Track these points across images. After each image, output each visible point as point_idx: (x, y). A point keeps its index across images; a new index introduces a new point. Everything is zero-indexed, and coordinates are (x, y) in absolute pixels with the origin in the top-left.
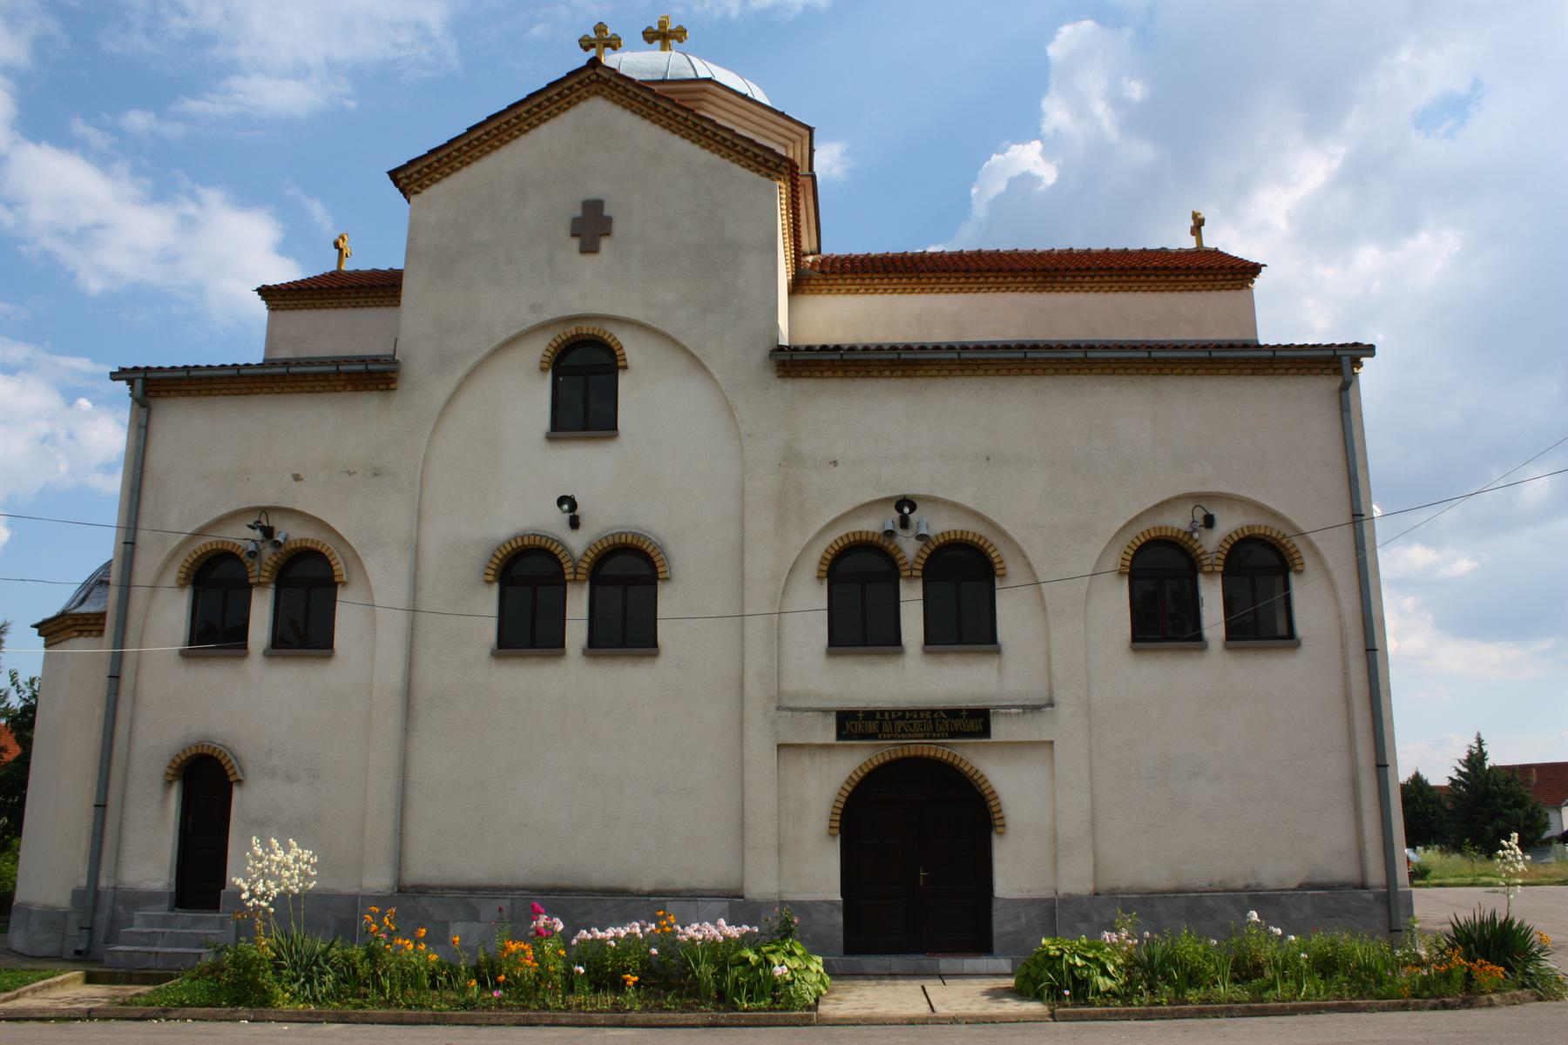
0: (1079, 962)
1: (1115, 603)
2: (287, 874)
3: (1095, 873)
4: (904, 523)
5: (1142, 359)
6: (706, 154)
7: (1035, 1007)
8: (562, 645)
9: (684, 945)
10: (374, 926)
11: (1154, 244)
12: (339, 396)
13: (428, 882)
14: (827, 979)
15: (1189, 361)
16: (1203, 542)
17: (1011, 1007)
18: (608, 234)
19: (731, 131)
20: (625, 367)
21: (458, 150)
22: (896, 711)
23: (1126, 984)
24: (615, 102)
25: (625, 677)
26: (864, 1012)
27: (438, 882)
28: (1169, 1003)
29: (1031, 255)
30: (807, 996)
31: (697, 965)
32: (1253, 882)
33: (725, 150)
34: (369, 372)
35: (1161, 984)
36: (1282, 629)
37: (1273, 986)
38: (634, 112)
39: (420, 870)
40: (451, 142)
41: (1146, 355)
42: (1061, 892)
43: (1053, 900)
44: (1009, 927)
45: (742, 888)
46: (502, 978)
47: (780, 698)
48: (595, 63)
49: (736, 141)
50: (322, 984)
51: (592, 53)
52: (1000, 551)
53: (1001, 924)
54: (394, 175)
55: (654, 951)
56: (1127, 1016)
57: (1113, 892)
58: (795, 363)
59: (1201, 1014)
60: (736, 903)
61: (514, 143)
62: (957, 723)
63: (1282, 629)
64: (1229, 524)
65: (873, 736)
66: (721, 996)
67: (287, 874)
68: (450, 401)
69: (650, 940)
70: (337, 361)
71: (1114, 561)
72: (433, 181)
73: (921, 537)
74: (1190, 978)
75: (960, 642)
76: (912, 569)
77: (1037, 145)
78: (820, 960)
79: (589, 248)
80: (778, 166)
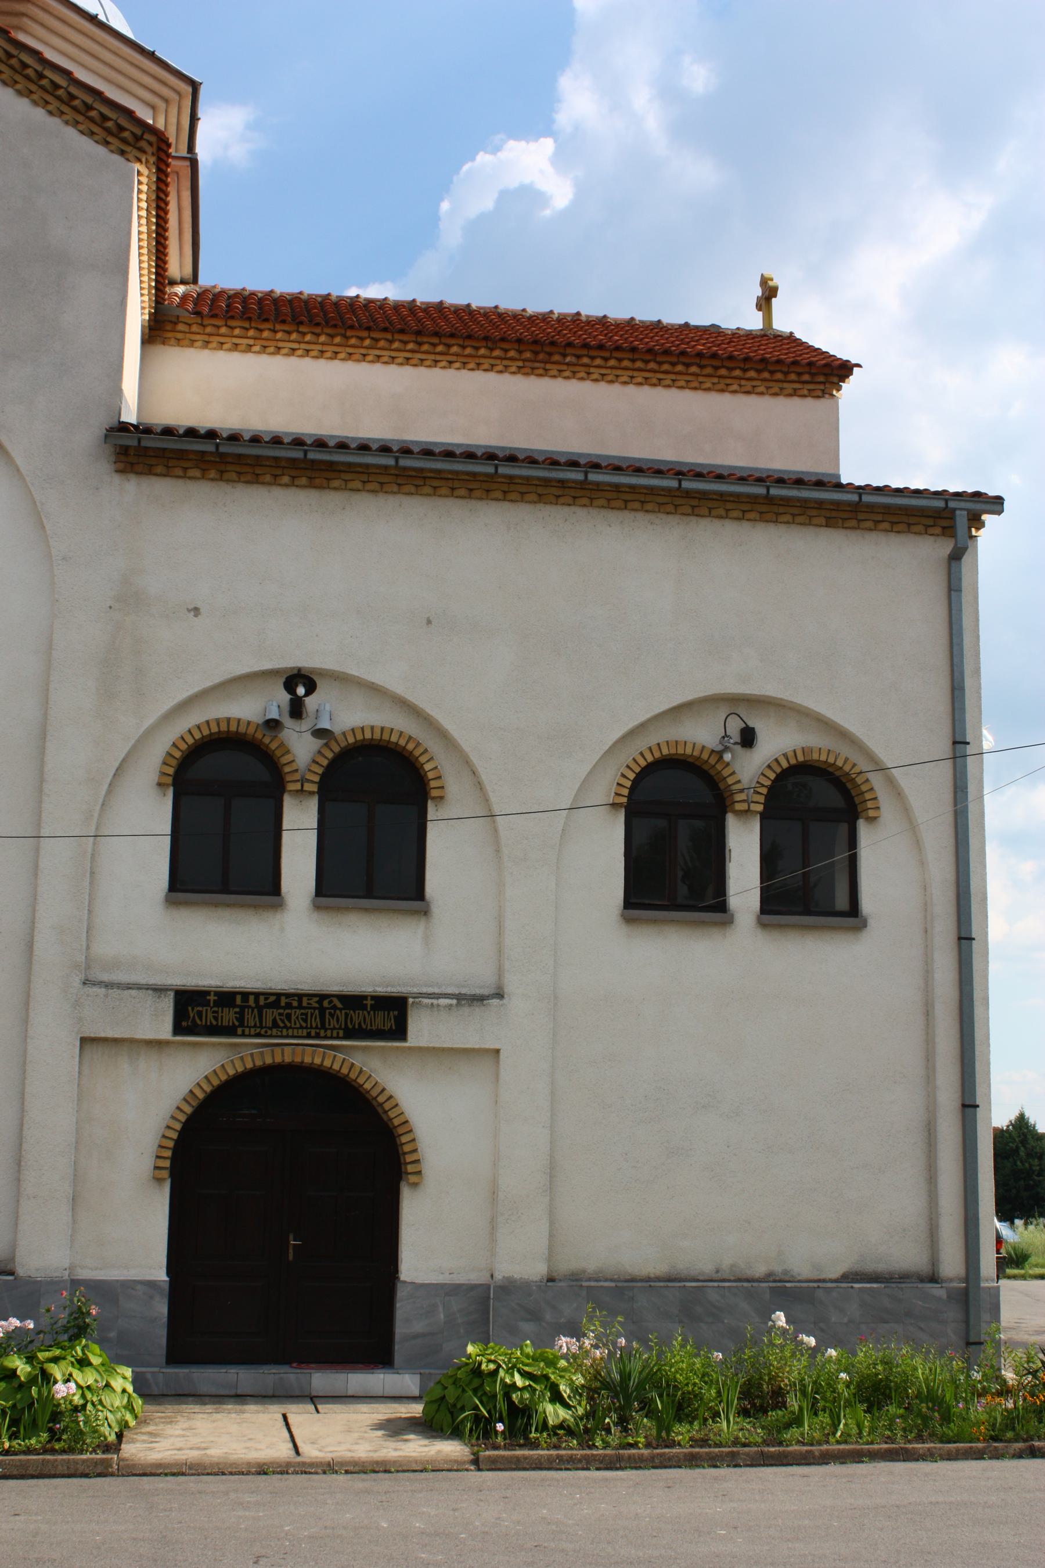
0: (519, 1381)
1: (603, 849)
3: (551, 1248)
4: (297, 710)
5: (668, 492)
6: (23, 105)
7: (451, 1449)
11: (700, 318)
14: (138, 1403)
15: (737, 498)
16: (737, 767)
17: (416, 1447)
19: (67, 74)
22: (267, 995)
23: (588, 1415)
26: (192, 1455)
28: (648, 1445)
29: (518, 318)
30: (105, 1430)
32: (778, 1269)
33: (55, 104)
35: (640, 1415)
36: (842, 902)
37: (797, 1421)
41: (674, 484)
42: (498, 1276)
43: (488, 1287)
44: (418, 1327)
47: (88, 967)
49: (73, 90)
52: (438, 762)
53: (408, 1321)
56: (586, 1464)
57: (576, 1278)
58: (143, 452)
59: (692, 1461)
62: (357, 1017)
63: (842, 902)
64: (777, 743)
65: (229, 1031)
71: (608, 785)
73: (319, 733)
74: (680, 1407)
75: (369, 894)
76: (303, 781)
77: (548, 145)
78: (128, 1372)
80: (138, 138)
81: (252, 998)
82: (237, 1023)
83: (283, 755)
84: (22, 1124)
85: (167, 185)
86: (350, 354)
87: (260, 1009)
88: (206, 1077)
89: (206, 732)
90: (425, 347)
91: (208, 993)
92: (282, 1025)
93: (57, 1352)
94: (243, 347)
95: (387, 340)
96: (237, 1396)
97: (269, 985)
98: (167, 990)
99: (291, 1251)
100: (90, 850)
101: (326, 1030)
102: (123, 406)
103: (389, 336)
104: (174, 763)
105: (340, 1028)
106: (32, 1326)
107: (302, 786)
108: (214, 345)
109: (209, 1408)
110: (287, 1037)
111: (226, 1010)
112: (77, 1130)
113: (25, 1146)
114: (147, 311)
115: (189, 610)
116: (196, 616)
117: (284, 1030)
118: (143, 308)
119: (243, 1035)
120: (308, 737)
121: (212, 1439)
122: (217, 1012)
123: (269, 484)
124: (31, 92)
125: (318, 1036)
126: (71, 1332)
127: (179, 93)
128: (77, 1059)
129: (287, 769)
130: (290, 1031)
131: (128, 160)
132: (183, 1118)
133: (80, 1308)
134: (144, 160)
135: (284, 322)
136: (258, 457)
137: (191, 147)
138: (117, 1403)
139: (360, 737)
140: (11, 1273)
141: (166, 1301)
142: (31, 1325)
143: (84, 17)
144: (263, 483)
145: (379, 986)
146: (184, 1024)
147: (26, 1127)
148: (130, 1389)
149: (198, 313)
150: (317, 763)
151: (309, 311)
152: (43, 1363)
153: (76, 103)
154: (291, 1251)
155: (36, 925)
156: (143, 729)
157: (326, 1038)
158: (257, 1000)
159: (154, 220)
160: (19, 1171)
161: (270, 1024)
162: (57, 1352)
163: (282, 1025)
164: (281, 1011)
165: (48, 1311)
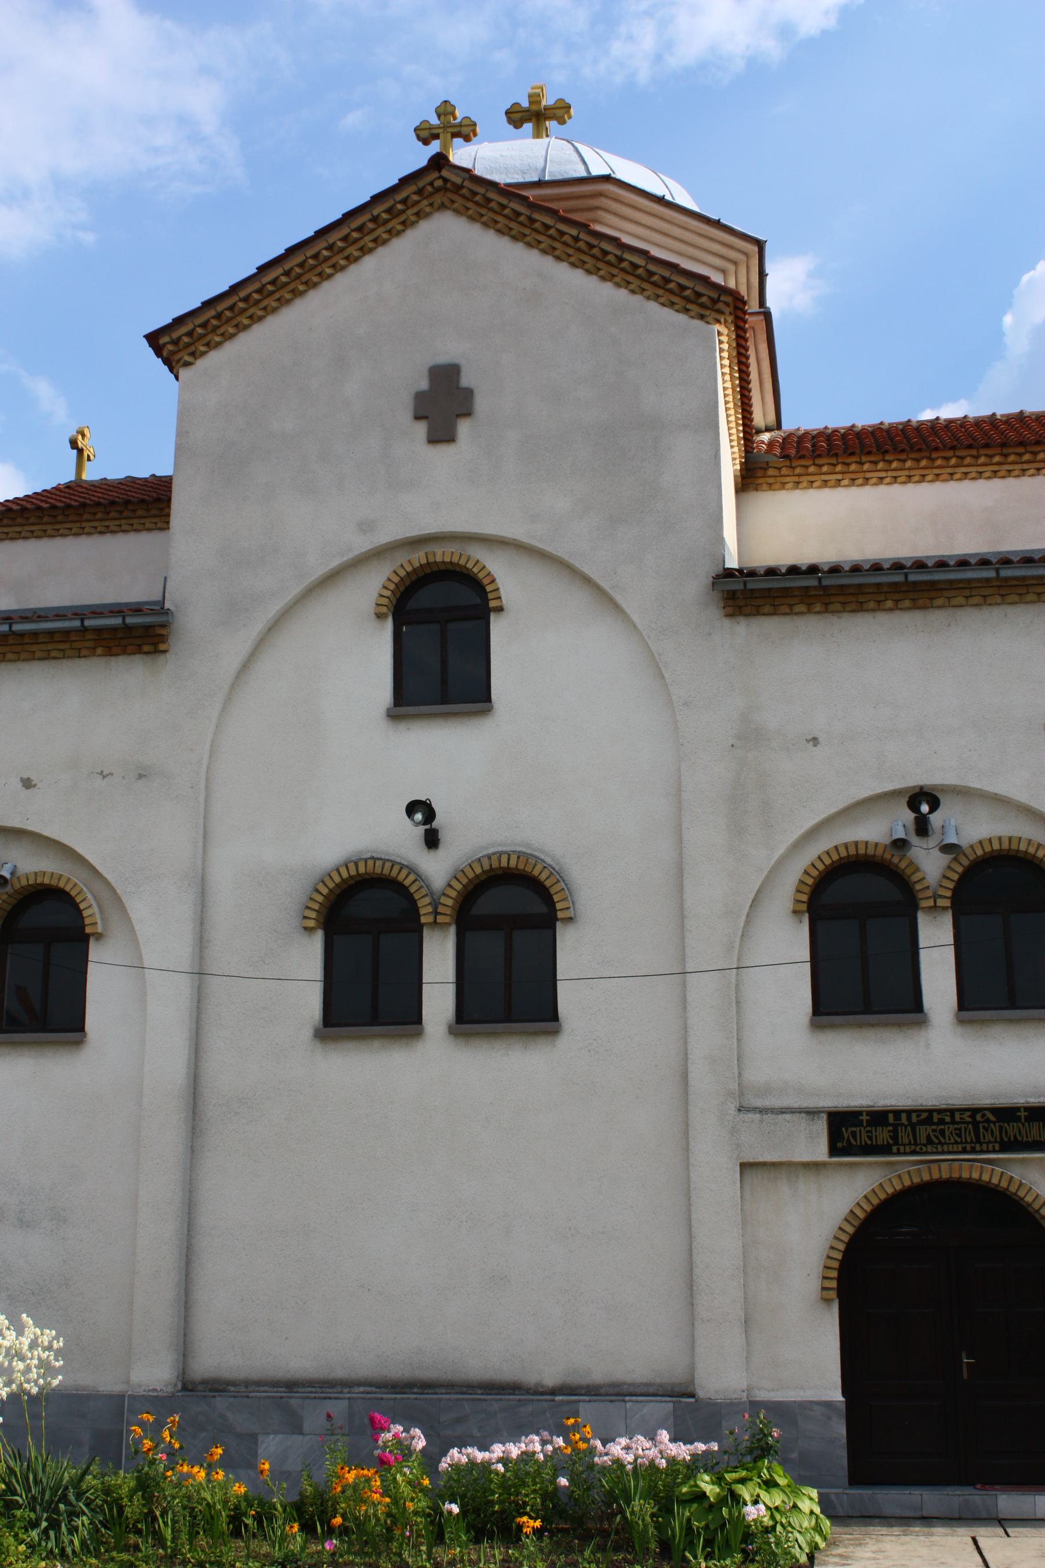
2: (20, 1366)
4: (922, 827)
8: (418, 1020)
9: (604, 1469)
10: (148, 1443)
12: (82, 663)
13: (226, 1374)
14: (826, 1524)
18: (468, 414)
19: (645, 253)
20: (500, 609)
21: (246, 300)
22: (919, 1112)
24: (472, 218)
25: (508, 1068)
27: (243, 1374)
30: (796, 1551)
31: (628, 1501)
33: (636, 283)
34: (127, 628)
38: (499, 231)
39: (218, 1356)
40: (234, 288)
45: (692, 1382)
46: (338, 1520)
47: (741, 1094)
48: (439, 161)
49: (652, 267)
50: (73, 1530)
51: (435, 147)
54: (153, 339)
55: (563, 1481)
58: (750, 595)
60: (684, 1405)
61: (326, 285)
62: (1012, 1129)
66: (666, 1549)
67: (20, 1366)
68: (246, 666)
69: (557, 1463)
70: (80, 613)
72: (211, 346)
73: (948, 848)
75: (1013, 1005)
76: (935, 897)
78: (814, 1493)
79: (442, 435)
80: (715, 302)
81: (904, 1116)
82: (891, 1142)
83: (913, 873)
84: (690, 1251)
85: (746, 340)
86: (938, 475)
87: (913, 1126)
88: (865, 1197)
89: (835, 857)
90: (1012, 458)
91: (860, 1113)
92: (936, 1141)
93: (744, 1473)
94: (832, 483)
95: (972, 456)
96: (923, 1518)
97: (920, 1102)
98: (820, 1112)
99: (965, 1370)
100: (733, 980)
101: (981, 1144)
102: (726, 553)
103: (974, 452)
104: (807, 890)
105: (996, 1141)
106: (716, 1448)
107: (935, 902)
108: (805, 484)
109: (896, 1530)
110: (943, 1153)
111: (879, 1129)
112: (744, 1253)
113: (696, 1271)
114: (738, 461)
115: (808, 741)
116: (815, 745)
117: (939, 1146)
118: (734, 459)
119: (898, 1153)
120: (936, 853)
121: (903, 1562)
122: (870, 1132)
123: (874, 610)
124: (614, 276)
125: (973, 1151)
126: (756, 1453)
127: (746, 254)
128: (738, 1184)
129: (918, 887)
130: (945, 1147)
131: (708, 323)
132: (846, 1238)
133: (761, 1429)
134: (722, 320)
135: (869, 453)
136: (860, 586)
137: (762, 301)
138: (806, 1524)
139: (988, 849)
140: (693, 1396)
141: (844, 1421)
142: (715, 1446)
143: (652, 200)
144: (867, 611)
145: (1031, 1097)
146: (839, 1145)
147: (695, 1251)
148: (817, 1510)
149: (786, 457)
150: (948, 878)
151: (892, 440)
152: (730, 1484)
153: (655, 278)
154: (965, 1370)
155: (689, 1056)
156: (774, 861)
157: (982, 1152)
158: (909, 1118)
159: (737, 375)
160: (692, 1296)
161: (924, 1141)
162: (744, 1473)
163: (936, 1141)
164: (935, 1127)
165: (732, 1433)
